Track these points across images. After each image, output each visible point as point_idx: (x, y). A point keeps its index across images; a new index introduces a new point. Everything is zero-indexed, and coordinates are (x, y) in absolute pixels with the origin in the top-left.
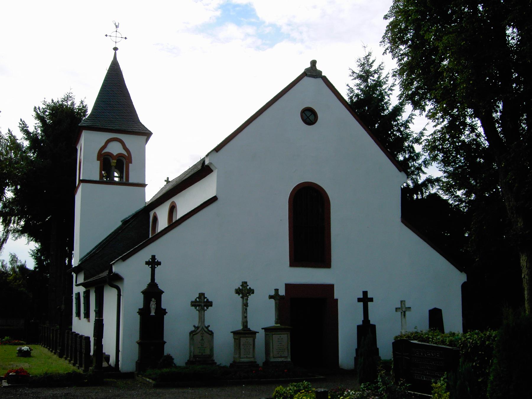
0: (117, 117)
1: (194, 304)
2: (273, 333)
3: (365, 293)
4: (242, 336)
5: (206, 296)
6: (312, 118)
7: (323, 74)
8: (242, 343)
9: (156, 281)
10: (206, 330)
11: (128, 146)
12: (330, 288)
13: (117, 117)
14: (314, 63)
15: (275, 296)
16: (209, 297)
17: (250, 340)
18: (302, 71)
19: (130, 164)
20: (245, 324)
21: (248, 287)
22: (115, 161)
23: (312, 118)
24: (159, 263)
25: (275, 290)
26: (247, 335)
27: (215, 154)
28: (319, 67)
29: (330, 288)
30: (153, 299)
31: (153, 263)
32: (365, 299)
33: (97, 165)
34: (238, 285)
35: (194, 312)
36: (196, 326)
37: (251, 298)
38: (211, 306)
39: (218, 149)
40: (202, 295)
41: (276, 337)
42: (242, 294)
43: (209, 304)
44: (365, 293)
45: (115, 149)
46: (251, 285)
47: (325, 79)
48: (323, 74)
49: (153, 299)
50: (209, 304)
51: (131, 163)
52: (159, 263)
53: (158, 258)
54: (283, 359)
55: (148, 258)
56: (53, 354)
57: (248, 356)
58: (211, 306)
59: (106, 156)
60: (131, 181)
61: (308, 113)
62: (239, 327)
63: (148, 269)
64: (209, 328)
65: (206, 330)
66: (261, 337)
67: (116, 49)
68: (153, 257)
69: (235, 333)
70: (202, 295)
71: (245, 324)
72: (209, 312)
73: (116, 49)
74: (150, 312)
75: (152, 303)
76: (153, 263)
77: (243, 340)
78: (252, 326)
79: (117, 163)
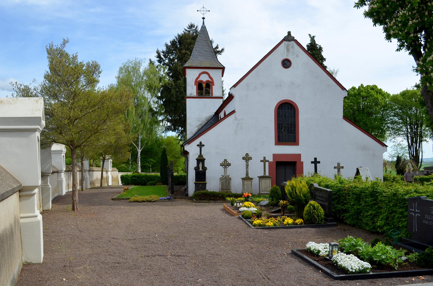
0: (205, 59)
1: (221, 165)
2: (262, 179)
3: (316, 159)
4: (245, 180)
5: (227, 161)
6: (288, 64)
7: (295, 39)
8: (245, 184)
9: (202, 154)
10: (227, 177)
11: (211, 76)
12: (299, 156)
13: (205, 59)
14: (289, 33)
15: (264, 161)
16: (229, 161)
17: (250, 182)
18: (283, 38)
19: (213, 86)
20: (247, 174)
21: (249, 156)
22: (205, 85)
23: (288, 64)
24: (203, 146)
25: (264, 157)
26: (248, 180)
27: (233, 89)
28: (292, 35)
29: (299, 156)
30: (201, 163)
31: (201, 145)
32: (316, 162)
33: (195, 87)
34: (244, 155)
35: (222, 168)
36: (223, 175)
37: (250, 162)
38: (230, 165)
39: (235, 86)
40: (225, 160)
41: (263, 181)
42: (246, 159)
43: (229, 165)
44: (316, 159)
45: (204, 78)
46: (250, 155)
47: (296, 41)
48: (295, 39)
49: (201, 163)
50: (229, 165)
51: (214, 85)
52: (203, 146)
53: (203, 143)
54: (267, 192)
55: (198, 143)
56: (377, 245)
57: (248, 190)
58: (230, 165)
59: (200, 83)
60: (214, 96)
61: (286, 62)
62: (244, 176)
63: (198, 148)
64: (229, 177)
65: (227, 177)
66: (256, 181)
67: (203, 18)
68: (201, 143)
69: (243, 179)
70: (225, 160)
71: (247, 174)
72: (229, 168)
73: (203, 18)
74: (199, 169)
75: (200, 164)
76: (201, 145)
77: (246, 182)
78: (250, 176)
79: (206, 86)
